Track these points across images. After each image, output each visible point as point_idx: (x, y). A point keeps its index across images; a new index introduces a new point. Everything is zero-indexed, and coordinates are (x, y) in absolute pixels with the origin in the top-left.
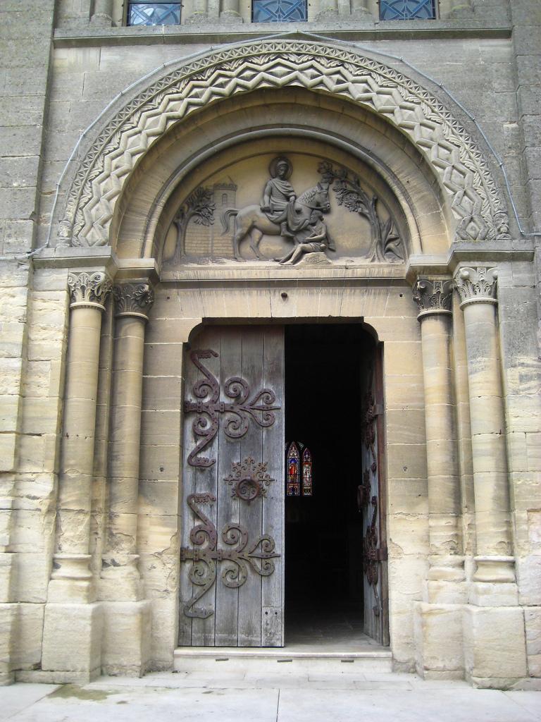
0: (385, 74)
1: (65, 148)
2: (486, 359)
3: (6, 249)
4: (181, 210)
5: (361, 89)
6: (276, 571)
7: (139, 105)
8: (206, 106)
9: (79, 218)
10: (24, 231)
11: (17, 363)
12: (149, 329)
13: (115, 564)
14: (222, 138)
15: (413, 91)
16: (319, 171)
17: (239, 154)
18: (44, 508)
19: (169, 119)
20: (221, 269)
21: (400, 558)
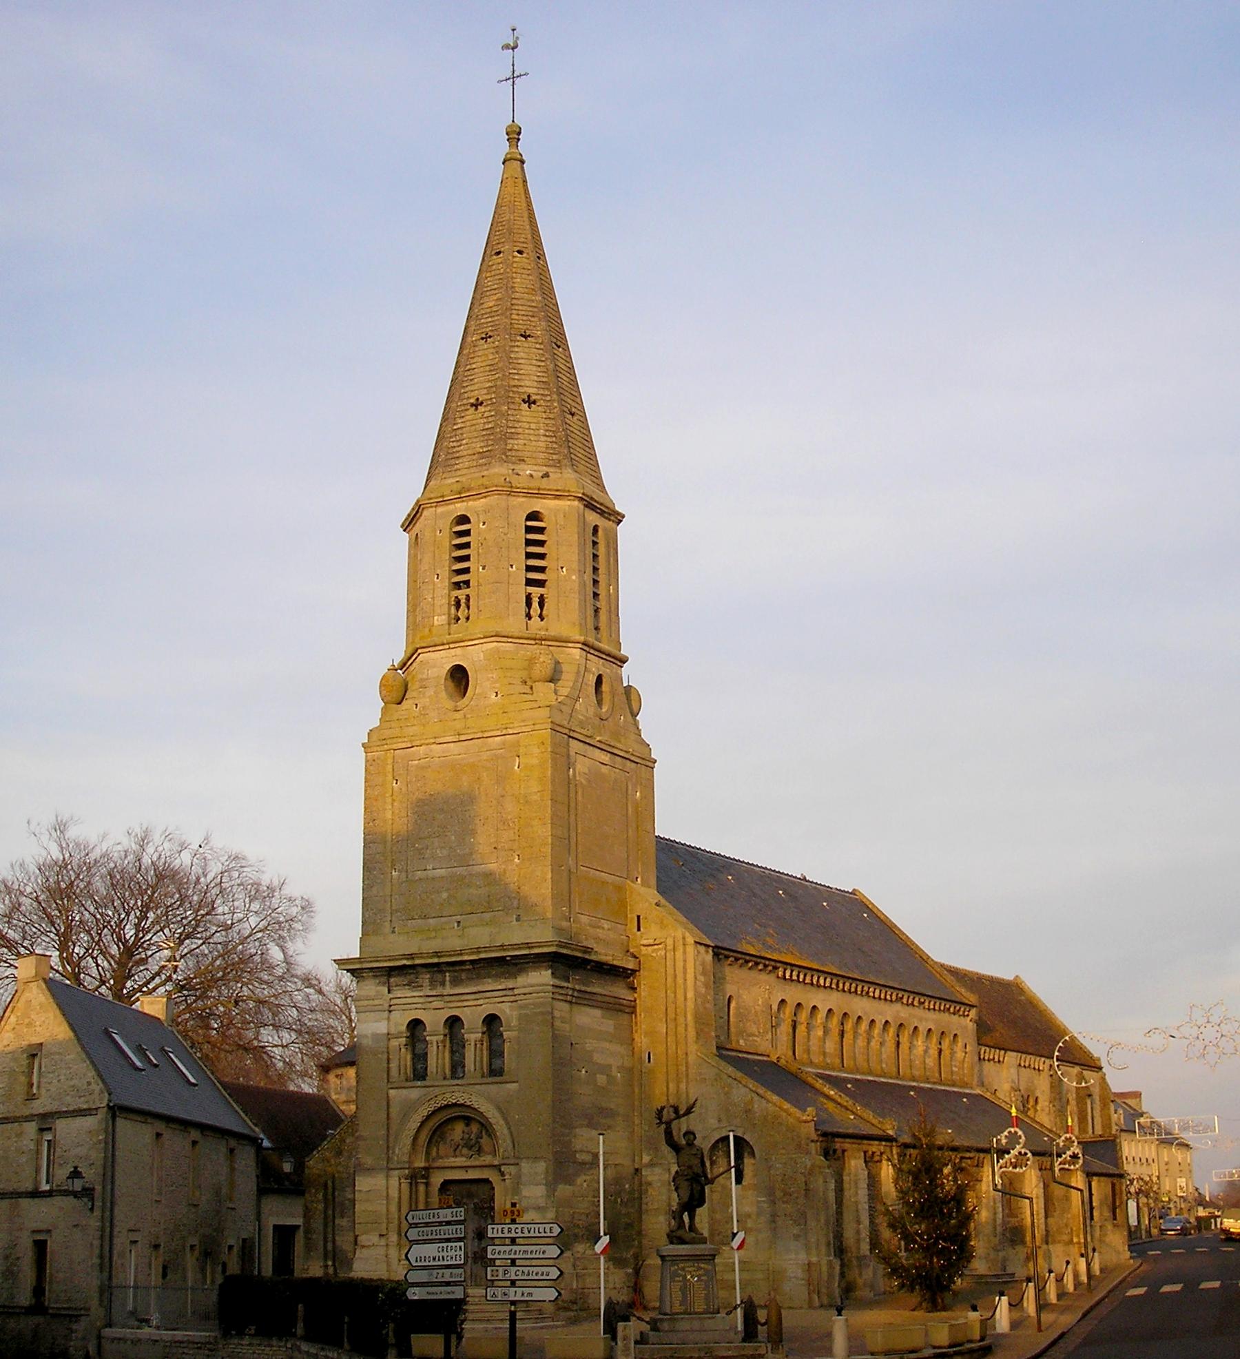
12: (427, 1184)
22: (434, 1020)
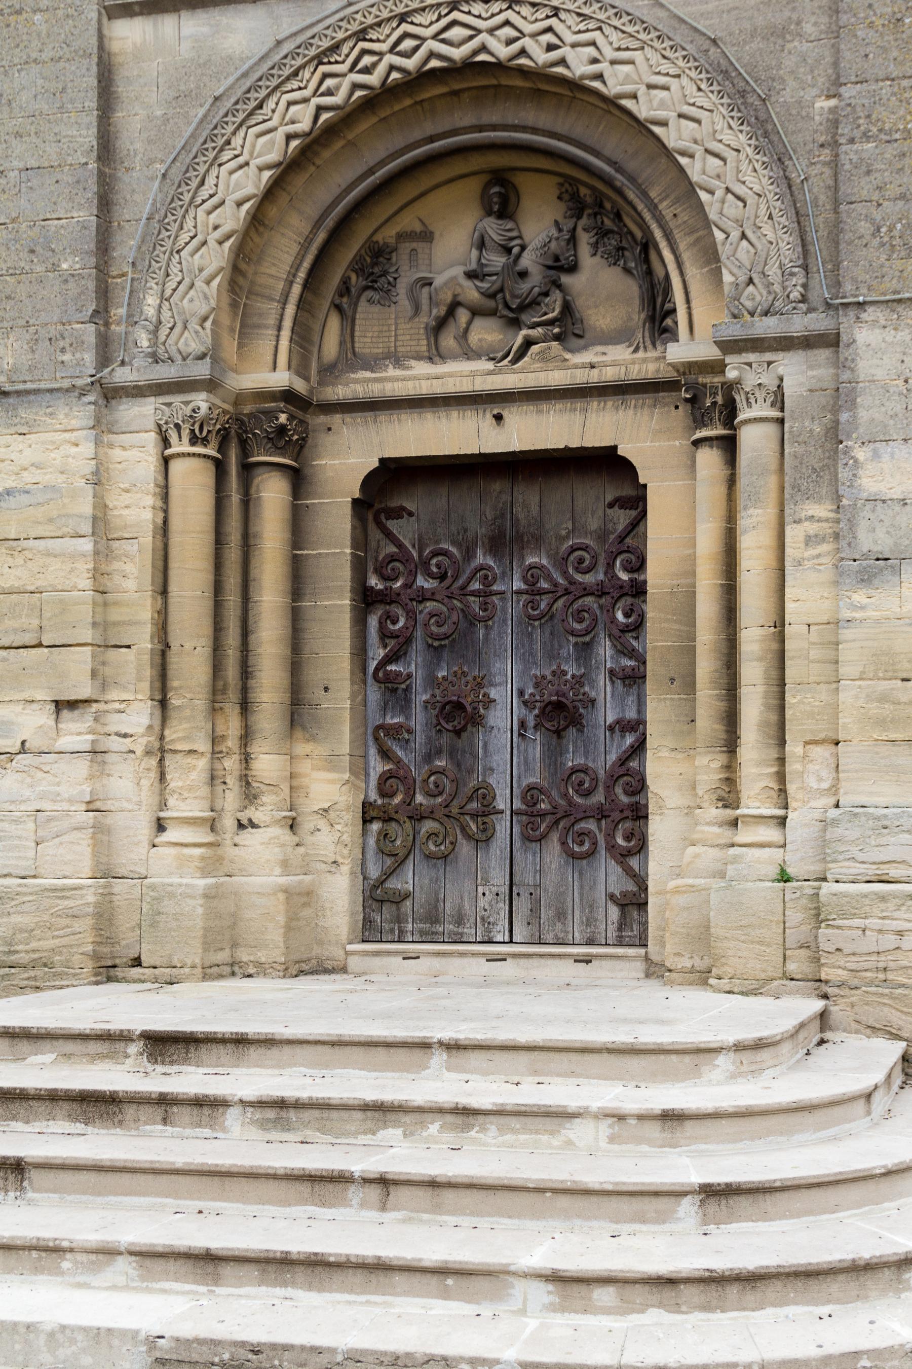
0: (624, 25)
1: (136, 197)
2: (760, 511)
3: (61, 371)
4: (345, 282)
5: (585, 59)
6: (498, 834)
7: (241, 116)
8: (348, 109)
9: (166, 314)
10: (83, 342)
11: (86, 545)
12: (298, 480)
13: (253, 825)
14: (388, 157)
15: (668, 53)
16: (560, 198)
17: (425, 181)
18: (139, 750)
19: (289, 137)
20: (404, 379)
21: (661, 814)
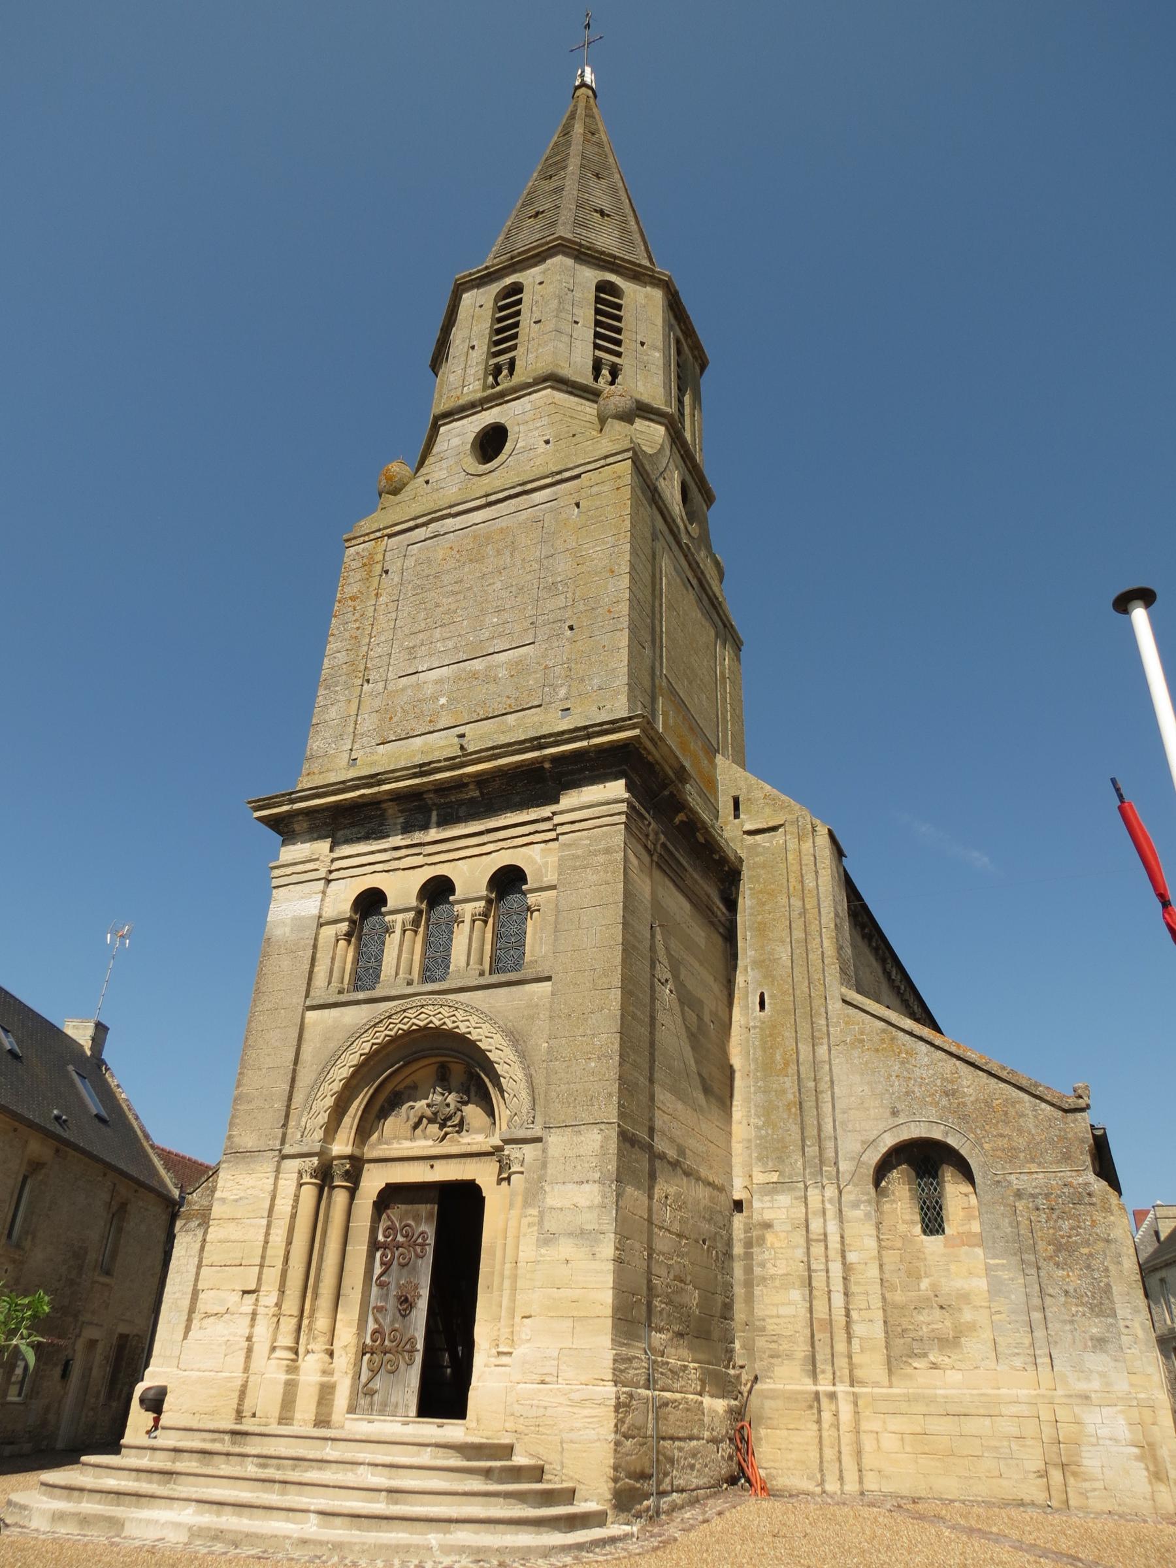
22: (402, 889)
